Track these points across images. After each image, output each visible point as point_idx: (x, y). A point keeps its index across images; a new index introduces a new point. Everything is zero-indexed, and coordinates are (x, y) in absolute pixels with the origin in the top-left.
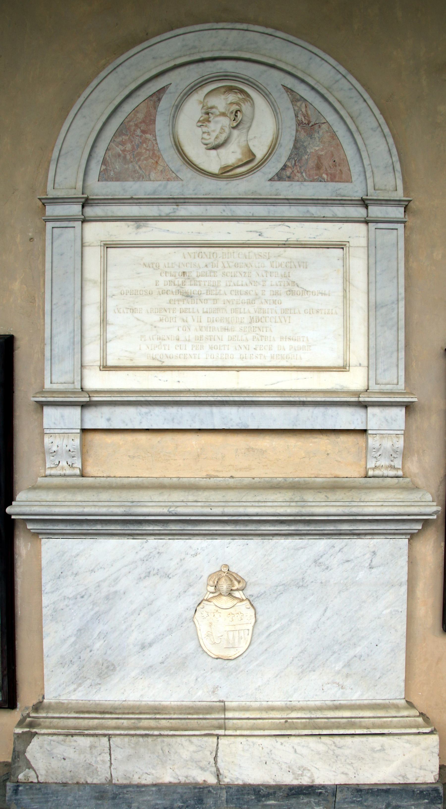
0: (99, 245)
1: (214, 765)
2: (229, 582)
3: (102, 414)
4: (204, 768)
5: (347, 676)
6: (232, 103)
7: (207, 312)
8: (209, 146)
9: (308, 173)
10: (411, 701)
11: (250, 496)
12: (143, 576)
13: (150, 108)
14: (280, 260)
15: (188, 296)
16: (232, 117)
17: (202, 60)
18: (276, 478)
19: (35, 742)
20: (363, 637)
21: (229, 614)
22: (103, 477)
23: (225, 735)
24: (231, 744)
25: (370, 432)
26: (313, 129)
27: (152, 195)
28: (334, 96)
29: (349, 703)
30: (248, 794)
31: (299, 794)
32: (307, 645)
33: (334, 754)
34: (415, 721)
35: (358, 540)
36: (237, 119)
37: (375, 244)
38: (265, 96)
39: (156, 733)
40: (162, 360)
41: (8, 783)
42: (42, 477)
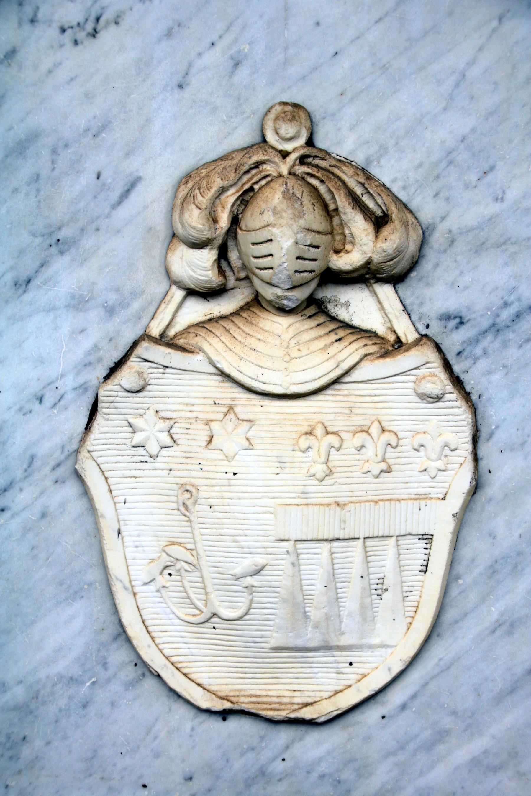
21: (310, 433)
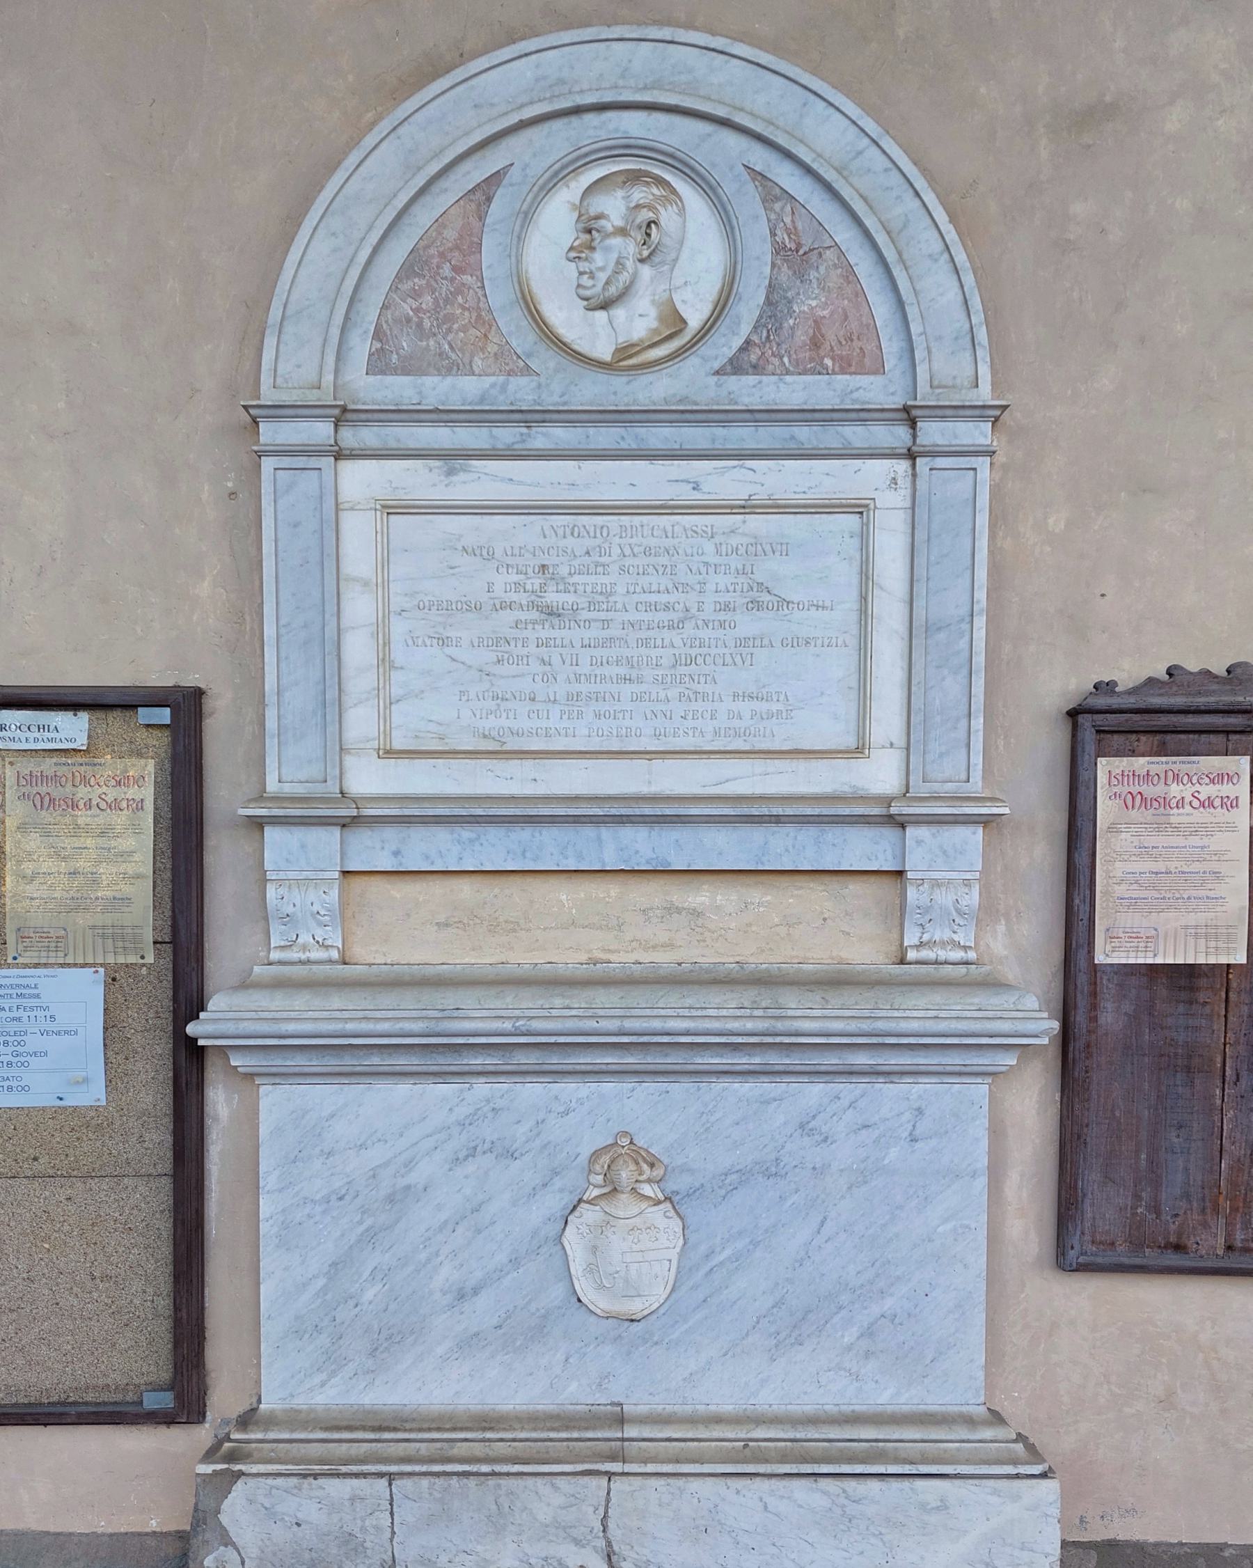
0: (371, 509)
1: (601, 1534)
3: (383, 842)
5: (868, 1355)
8: (591, 301)
9: (794, 356)
12: (461, 1156)
13: (471, 218)
14: (734, 541)
16: (640, 237)
17: (577, 111)
20: (898, 1278)
23: (623, 1474)
25: (910, 875)
26: (807, 262)
27: (476, 404)
29: (872, 1409)
39: (485, 1468)
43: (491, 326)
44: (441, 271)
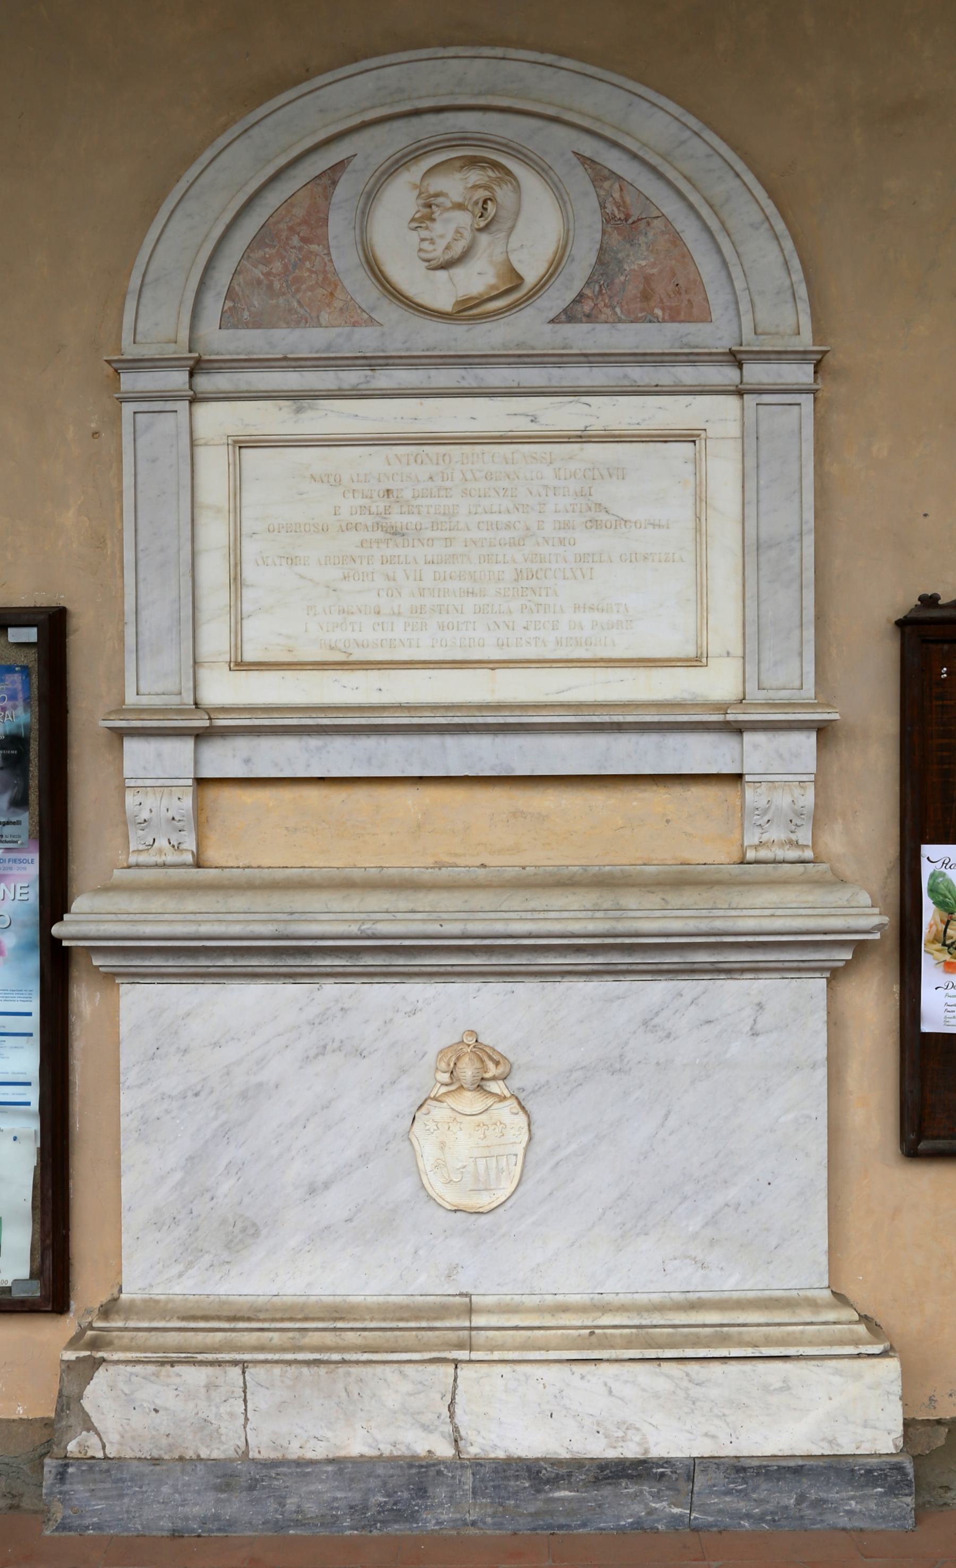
0: (224, 444)
1: (449, 1420)
2: (478, 1064)
4: (428, 1426)
5: (712, 1242)
6: (475, 187)
7: (433, 563)
8: (432, 263)
9: (626, 307)
10: (843, 1292)
11: (516, 901)
12: (312, 1053)
15: (396, 532)
16: (478, 211)
17: (417, 113)
18: (568, 866)
19: (101, 1375)
21: (479, 1125)
22: (238, 867)
23: (470, 1361)
24: (482, 1377)
25: (747, 778)
27: (323, 351)
28: (675, 168)
29: (717, 1296)
30: (517, 1478)
31: (620, 1477)
32: (632, 1184)
33: (687, 1397)
34: (851, 1331)
35: (729, 981)
36: (486, 215)
37: (757, 433)
38: (541, 172)
39: (336, 1357)
40: (349, 651)
41: (47, 1461)
42: (123, 868)
43: (336, 286)
44: (290, 242)
